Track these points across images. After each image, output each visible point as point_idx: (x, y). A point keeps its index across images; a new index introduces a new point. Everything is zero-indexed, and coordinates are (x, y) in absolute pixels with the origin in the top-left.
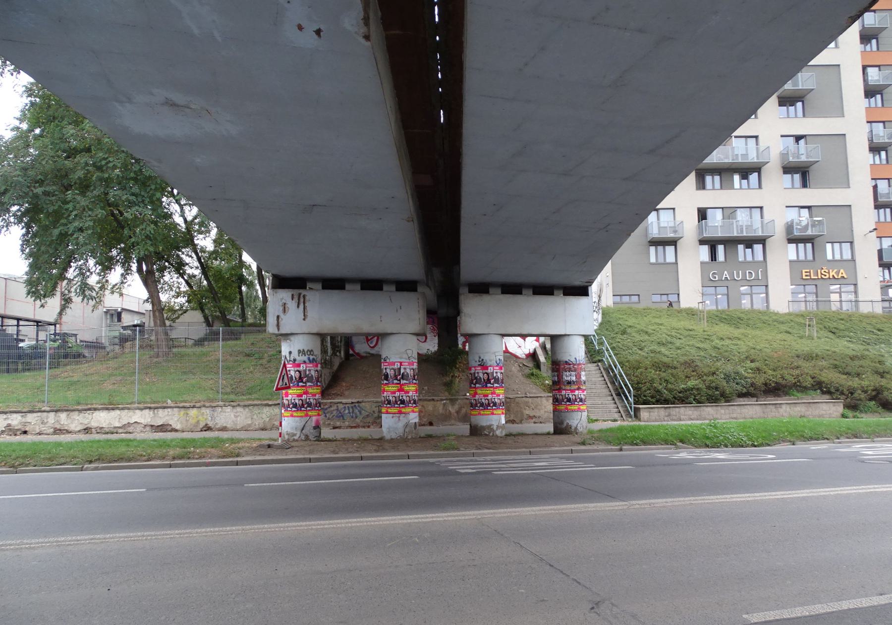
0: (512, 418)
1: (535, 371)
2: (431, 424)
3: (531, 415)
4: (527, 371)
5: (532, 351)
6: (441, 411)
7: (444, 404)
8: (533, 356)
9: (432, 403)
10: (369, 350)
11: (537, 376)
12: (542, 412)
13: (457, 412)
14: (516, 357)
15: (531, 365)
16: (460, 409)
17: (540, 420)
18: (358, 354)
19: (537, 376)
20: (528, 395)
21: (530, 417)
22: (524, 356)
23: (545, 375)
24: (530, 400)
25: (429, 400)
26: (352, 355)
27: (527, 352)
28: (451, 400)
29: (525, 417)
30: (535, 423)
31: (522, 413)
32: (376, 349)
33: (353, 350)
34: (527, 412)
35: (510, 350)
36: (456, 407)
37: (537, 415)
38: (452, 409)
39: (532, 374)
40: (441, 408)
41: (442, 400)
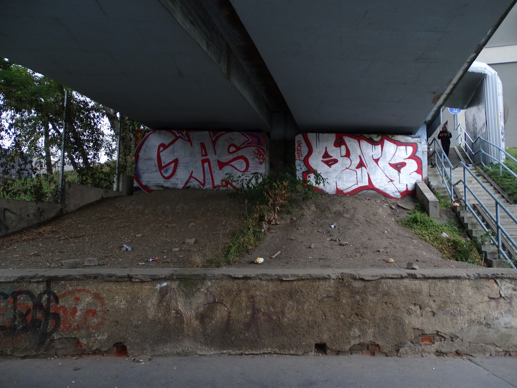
0: (369, 338)
1: (418, 214)
2: (121, 349)
3: (429, 330)
4: (404, 215)
5: (410, 188)
6: (151, 313)
7: (163, 293)
8: (413, 194)
9: (126, 287)
10: (161, 181)
11: (424, 225)
12: (462, 322)
13: (202, 317)
14: (386, 195)
15: (410, 206)
16: (211, 306)
17: (457, 346)
18: (146, 188)
19: (424, 225)
20: (419, 271)
21: (424, 337)
22: (398, 195)
23: (437, 222)
24: (425, 285)
25: (119, 280)
26: (137, 189)
27: (403, 188)
28: (183, 279)
29: (411, 335)
30: (439, 353)
31: (400, 323)
32: (173, 180)
33: (139, 182)
34: (415, 321)
35: (376, 185)
36: (200, 300)
37: (447, 330)
38: (187, 307)
39: (415, 221)
40: (152, 303)
41: (155, 279)
